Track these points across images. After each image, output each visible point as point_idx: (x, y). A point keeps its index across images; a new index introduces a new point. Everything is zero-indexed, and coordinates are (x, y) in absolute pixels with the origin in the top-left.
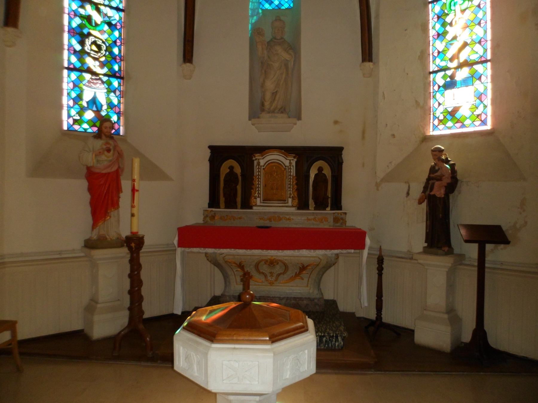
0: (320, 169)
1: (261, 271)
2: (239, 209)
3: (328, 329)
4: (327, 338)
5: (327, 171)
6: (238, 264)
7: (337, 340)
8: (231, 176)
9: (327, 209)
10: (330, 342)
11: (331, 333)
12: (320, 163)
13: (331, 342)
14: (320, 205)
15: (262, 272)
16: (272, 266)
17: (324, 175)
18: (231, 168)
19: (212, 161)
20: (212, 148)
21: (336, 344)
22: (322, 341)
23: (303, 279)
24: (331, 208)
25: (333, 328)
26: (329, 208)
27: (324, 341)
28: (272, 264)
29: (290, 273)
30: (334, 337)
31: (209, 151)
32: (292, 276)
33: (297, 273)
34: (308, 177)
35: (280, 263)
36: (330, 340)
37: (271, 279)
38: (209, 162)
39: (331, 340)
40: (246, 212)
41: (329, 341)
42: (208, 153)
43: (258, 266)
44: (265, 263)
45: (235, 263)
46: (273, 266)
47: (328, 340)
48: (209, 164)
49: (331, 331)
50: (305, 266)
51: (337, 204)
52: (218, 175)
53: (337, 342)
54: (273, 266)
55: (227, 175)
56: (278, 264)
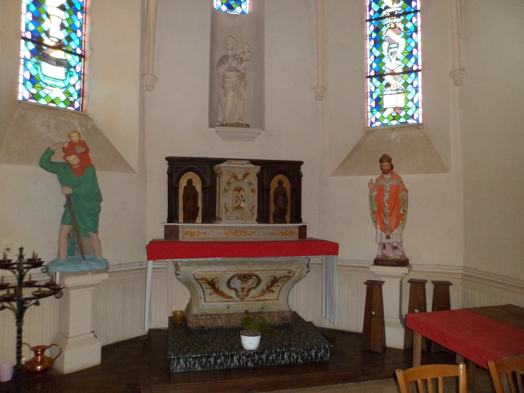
0: (190, 182)
1: (232, 287)
2: (288, 224)
3: (169, 351)
4: (273, 357)
5: (287, 185)
6: (210, 281)
7: (178, 363)
8: (281, 191)
9: (197, 221)
10: (325, 356)
11: (173, 355)
12: (190, 175)
13: (172, 366)
14: (280, 218)
15: (233, 288)
16: (245, 281)
17: (284, 189)
18: (190, 182)
19: (170, 174)
20: (170, 160)
21: (177, 367)
22: (217, 364)
23: (273, 292)
24: (202, 220)
25: (278, 344)
26: (199, 219)
27: (319, 357)
28: (245, 279)
29: (263, 286)
30: (176, 360)
31: (167, 162)
32: (263, 290)
33: (269, 286)
34: (269, 189)
35: (253, 277)
36: (324, 355)
37: (241, 295)
38: (167, 174)
39: (226, 362)
40: (212, 226)
41: (275, 359)
42: (165, 166)
43: (258, 280)
44: (238, 278)
45: (206, 280)
46: (246, 280)
47: (274, 359)
48: (167, 176)
49: (172, 353)
50: (277, 278)
51: (297, 217)
52: (177, 188)
53: (283, 360)
54: (246, 280)
55: (276, 190)
56: (251, 278)
